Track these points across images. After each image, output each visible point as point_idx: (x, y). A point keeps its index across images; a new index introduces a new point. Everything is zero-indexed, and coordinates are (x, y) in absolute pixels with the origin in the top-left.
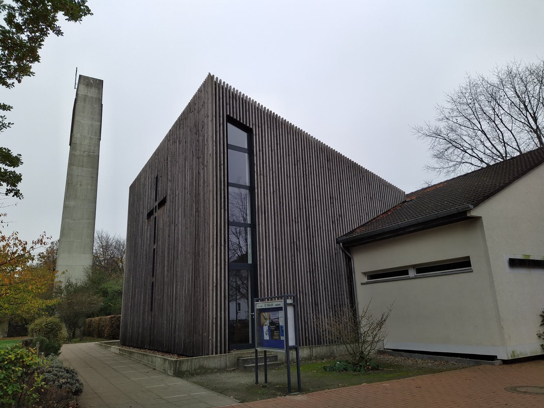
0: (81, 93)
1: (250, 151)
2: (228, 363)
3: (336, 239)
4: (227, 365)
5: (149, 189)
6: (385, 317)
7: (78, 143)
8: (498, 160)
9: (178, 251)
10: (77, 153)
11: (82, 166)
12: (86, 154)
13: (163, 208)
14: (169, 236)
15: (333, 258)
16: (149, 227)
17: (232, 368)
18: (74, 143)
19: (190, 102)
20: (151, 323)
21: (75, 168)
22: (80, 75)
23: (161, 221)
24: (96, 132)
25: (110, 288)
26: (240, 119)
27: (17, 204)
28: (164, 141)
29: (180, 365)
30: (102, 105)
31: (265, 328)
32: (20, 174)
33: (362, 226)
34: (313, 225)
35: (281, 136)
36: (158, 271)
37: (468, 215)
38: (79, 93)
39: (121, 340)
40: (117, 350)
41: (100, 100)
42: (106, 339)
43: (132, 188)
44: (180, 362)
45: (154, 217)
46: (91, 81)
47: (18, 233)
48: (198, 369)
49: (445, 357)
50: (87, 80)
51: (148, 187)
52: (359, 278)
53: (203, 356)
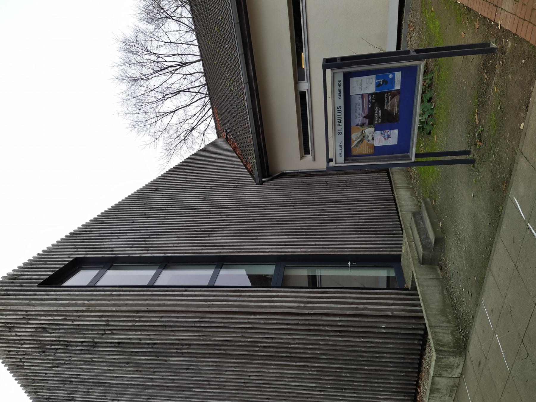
2: (431, 277)
3: (257, 185)
4: (435, 277)
8: (207, 102)
15: (280, 188)
17: (437, 271)
29: (443, 345)
34: (235, 202)
44: (439, 344)
48: (447, 317)
49: (401, 45)
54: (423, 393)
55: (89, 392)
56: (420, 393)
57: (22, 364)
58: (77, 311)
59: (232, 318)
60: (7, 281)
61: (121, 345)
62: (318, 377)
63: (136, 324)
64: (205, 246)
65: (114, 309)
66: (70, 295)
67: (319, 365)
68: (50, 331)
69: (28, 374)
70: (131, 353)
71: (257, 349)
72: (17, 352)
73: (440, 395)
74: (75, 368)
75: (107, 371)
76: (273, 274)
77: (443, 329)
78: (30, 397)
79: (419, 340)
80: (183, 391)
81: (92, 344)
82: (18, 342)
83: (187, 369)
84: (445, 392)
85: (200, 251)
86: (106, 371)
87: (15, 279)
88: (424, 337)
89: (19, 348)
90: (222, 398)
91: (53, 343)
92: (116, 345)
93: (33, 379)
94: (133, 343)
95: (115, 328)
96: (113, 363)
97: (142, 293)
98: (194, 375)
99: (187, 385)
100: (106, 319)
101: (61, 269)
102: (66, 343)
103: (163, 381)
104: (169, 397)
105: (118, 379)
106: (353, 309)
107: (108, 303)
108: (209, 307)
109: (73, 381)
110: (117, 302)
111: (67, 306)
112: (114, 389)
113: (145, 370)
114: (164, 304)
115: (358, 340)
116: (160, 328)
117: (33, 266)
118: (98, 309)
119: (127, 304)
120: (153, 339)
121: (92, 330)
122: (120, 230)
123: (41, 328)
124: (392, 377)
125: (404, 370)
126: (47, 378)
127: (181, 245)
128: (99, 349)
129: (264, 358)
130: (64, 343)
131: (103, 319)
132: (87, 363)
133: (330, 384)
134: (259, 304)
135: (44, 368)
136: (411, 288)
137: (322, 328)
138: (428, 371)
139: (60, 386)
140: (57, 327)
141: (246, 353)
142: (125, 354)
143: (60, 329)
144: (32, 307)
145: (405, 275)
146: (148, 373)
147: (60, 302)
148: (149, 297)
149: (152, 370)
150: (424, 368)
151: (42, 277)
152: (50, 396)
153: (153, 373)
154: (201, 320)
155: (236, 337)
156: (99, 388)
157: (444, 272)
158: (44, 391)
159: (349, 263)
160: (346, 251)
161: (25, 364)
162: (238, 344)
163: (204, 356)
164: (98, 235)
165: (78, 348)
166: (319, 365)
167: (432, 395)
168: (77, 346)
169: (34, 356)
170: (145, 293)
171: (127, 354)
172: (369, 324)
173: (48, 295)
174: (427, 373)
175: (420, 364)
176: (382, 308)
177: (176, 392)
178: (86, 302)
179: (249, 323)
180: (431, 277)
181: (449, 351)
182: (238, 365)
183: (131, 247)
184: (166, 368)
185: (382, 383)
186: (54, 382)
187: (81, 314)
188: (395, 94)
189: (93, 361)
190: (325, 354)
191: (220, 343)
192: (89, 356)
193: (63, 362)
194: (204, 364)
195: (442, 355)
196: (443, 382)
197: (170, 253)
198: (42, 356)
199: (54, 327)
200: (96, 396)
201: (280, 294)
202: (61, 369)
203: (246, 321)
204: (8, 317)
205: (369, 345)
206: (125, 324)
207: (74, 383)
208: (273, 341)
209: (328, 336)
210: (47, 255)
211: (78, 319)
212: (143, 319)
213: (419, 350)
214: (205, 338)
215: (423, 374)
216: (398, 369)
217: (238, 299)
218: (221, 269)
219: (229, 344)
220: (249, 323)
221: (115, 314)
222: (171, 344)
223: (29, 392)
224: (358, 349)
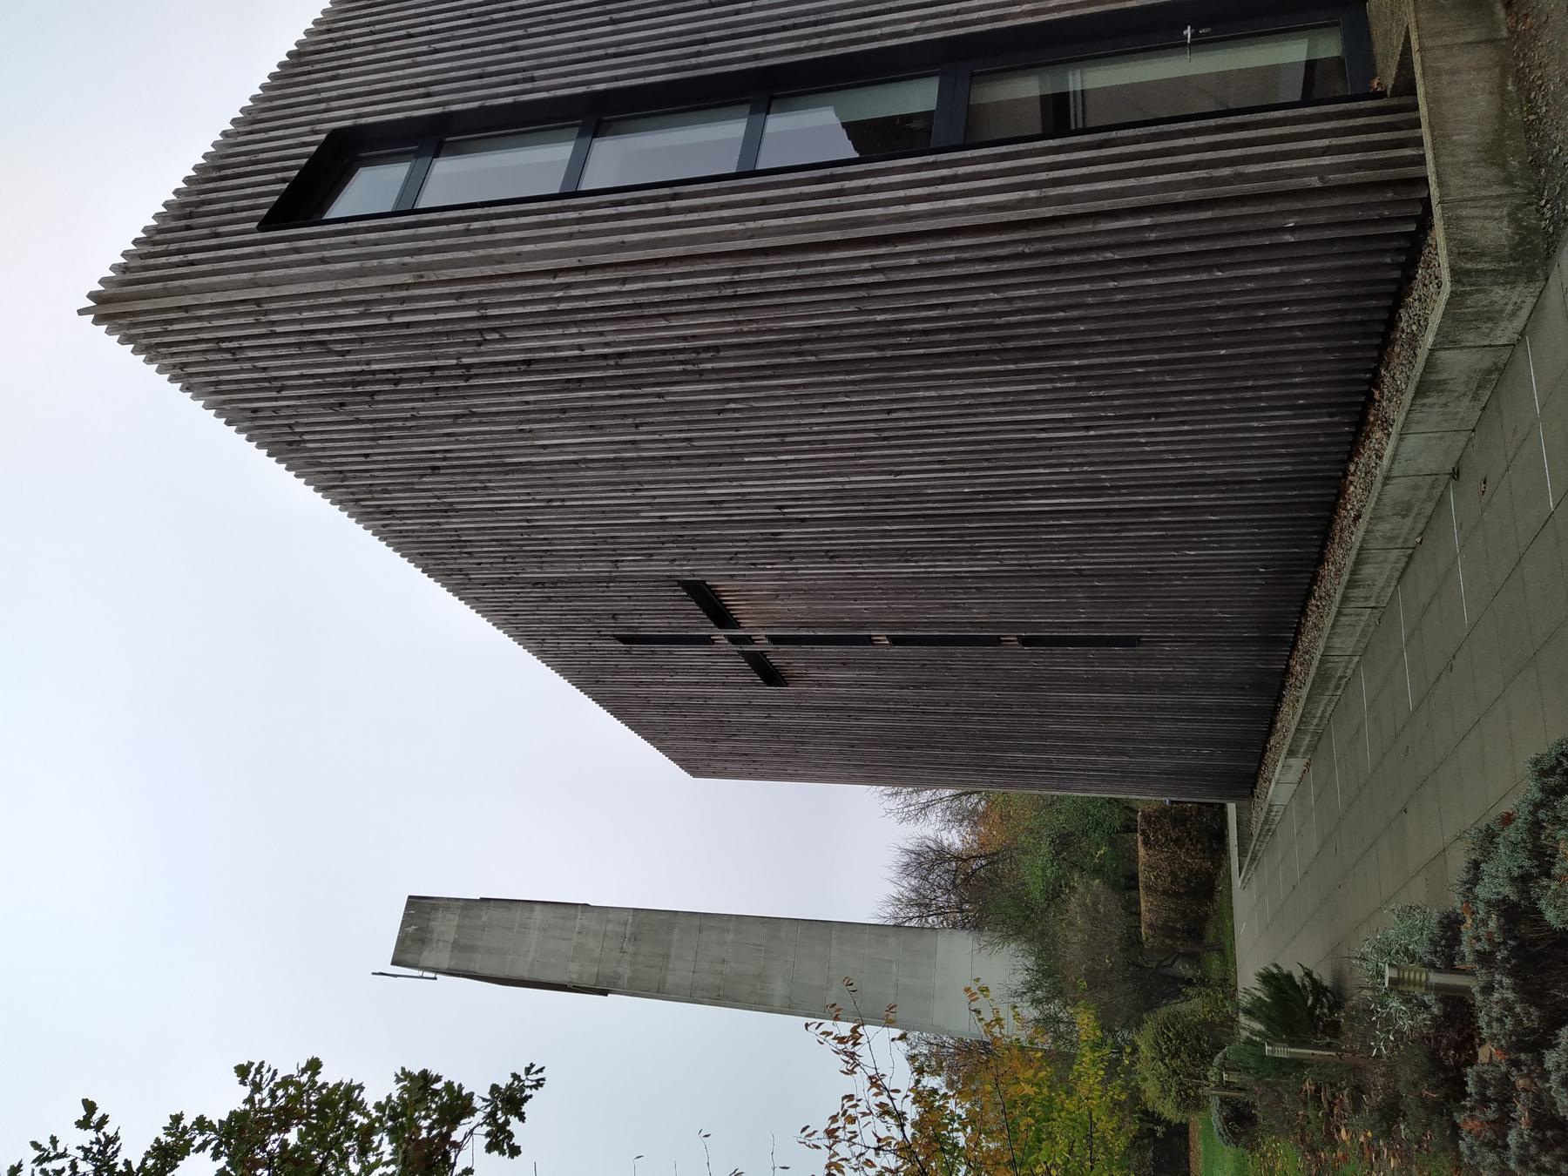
0: (445, 961)
4: (1484, 37)
5: (678, 678)
7: (595, 970)
9: (889, 494)
10: (626, 971)
11: (666, 956)
12: (631, 948)
13: (729, 600)
14: (832, 556)
16: (815, 674)
18: (597, 980)
19: (244, 436)
20: (1185, 640)
21: (670, 979)
22: (394, 963)
23: (777, 606)
24: (562, 918)
25: (1044, 871)
26: (284, 180)
27: (703, 1133)
28: (476, 602)
29: (1479, 255)
30: (482, 900)
32: (398, 1080)
35: (378, 27)
36: (975, 612)
38: (445, 966)
39: (1233, 798)
40: (1290, 767)
41: (468, 904)
42: (1220, 866)
43: (696, 766)
45: (771, 648)
46: (411, 929)
47: (808, 1127)
48: (1504, 166)
50: (408, 942)
51: (669, 684)
53: (1424, 181)
54: (1390, 402)
55: (486, 488)
56: (1379, 401)
57: (297, 438)
58: (393, 287)
59: (823, 263)
60: (173, 224)
61: (534, 367)
62: (1080, 394)
63: (559, 308)
64: (706, 41)
65: (488, 270)
66: (355, 244)
67: (1084, 362)
68: (338, 347)
69: (322, 461)
70: (566, 385)
71: (904, 340)
72: (275, 410)
73: (1443, 400)
74: (435, 436)
75: (518, 436)
76: (933, 107)
77: (1486, 207)
78: (346, 513)
79: (1398, 251)
80: (720, 464)
81: (459, 372)
82: (267, 385)
83: (720, 412)
84: (1462, 389)
85: (694, 61)
86: (514, 436)
87: (190, 216)
88: (1414, 247)
89: (276, 399)
90: (820, 472)
91: (359, 378)
92: (523, 368)
93: (341, 472)
94: (566, 359)
95: (507, 322)
96: (525, 415)
97: (551, 217)
98: (741, 424)
99: (728, 451)
100: (475, 301)
101: (304, 170)
102: (391, 376)
103: (663, 445)
104: (687, 481)
105: (547, 451)
106: (1196, 183)
107: (467, 254)
108: (751, 237)
109: (438, 468)
110: (492, 251)
111: (360, 276)
112: (546, 475)
113: (612, 422)
114: (623, 242)
115: (1205, 276)
116: (625, 313)
117: (223, 173)
118: (445, 274)
119: (519, 254)
120: (615, 342)
121: (447, 334)
122: (431, 23)
123: (311, 342)
124: (1300, 369)
125: (1339, 344)
126: (374, 467)
127: (630, 48)
128: (480, 382)
129: (928, 362)
130: (386, 376)
131: (469, 301)
132: (460, 421)
133: (1114, 408)
134: (901, 209)
135: (357, 443)
136: (1394, 86)
137: (1094, 257)
138: (1414, 339)
139: (410, 480)
140: (353, 336)
141: (874, 354)
142: (550, 387)
143: (362, 341)
144: (267, 289)
145: (1379, 48)
146: (621, 430)
147: (339, 266)
148: (576, 228)
149: (629, 421)
150: (1403, 331)
151: (262, 201)
152: (393, 505)
153: (633, 430)
154: (736, 278)
156: (507, 477)
157: (1517, 13)
158: (376, 496)
159: (1188, 32)
161: (306, 437)
162: (847, 332)
163: (758, 372)
164: (370, 48)
165: (425, 385)
166: (1084, 362)
167: (1419, 402)
168: (421, 380)
169: (320, 415)
170: (560, 216)
171: (557, 386)
172: (1243, 226)
173: (297, 251)
174: (1410, 344)
175: (1391, 323)
176: (1291, 169)
177: (701, 469)
178: (407, 259)
179: (874, 270)
180: (1471, 36)
181: (1493, 270)
182: (856, 388)
183: (480, 76)
184: (665, 414)
185: (1266, 388)
186: (394, 474)
187: (404, 293)
189: (473, 414)
190: (1100, 332)
191: (798, 336)
192: (461, 402)
193: (400, 424)
194: (763, 394)
195: (1471, 285)
196: (1458, 363)
197: (601, 79)
198: (341, 414)
199: (346, 336)
200: (505, 495)
201: (961, 170)
202: (400, 441)
203: (866, 265)
204: (216, 323)
205: (1236, 287)
206: (528, 309)
207: (442, 471)
208: (950, 312)
209: (1113, 278)
210: (251, 133)
211: (400, 308)
212: (574, 292)
213: (1393, 281)
214: (754, 326)
215: (1397, 349)
216: (1318, 345)
217: (835, 201)
218: (768, 113)
219: (823, 334)
220: (874, 270)
221: (496, 285)
222: (664, 352)
223: (341, 502)
224: (1204, 303)
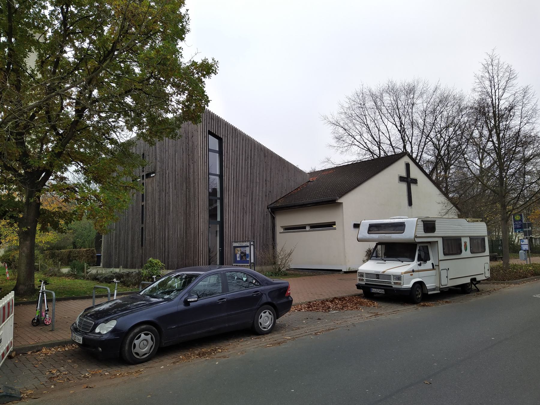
1: (220, 152)
6: (292, 251)
31: (238, 255)
33: (282, 198)
37: (336, 202)
52: (279, 229)
155: (192, 210)
160: (225, 248)
188: (246, 259)
